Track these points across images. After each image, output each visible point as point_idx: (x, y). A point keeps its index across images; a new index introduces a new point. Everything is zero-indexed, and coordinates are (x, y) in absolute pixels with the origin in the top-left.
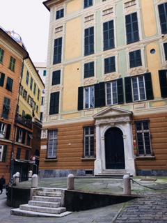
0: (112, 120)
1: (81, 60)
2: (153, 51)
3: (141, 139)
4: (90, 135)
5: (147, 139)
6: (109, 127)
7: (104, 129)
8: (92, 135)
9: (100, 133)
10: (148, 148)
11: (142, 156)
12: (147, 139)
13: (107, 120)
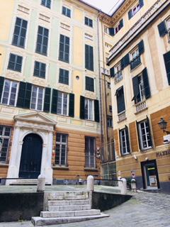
0: (36, 125)
1: (7, 47)
2: (77, 77)
4: (61, 143)
5: (63, 151)
6: (31, 132)
7: (26, 132)
8: (57, 143)
9: (18, 138)
10: (63, 159)
11: (57, 166)
12: (63, 151)
13: (31, 124)
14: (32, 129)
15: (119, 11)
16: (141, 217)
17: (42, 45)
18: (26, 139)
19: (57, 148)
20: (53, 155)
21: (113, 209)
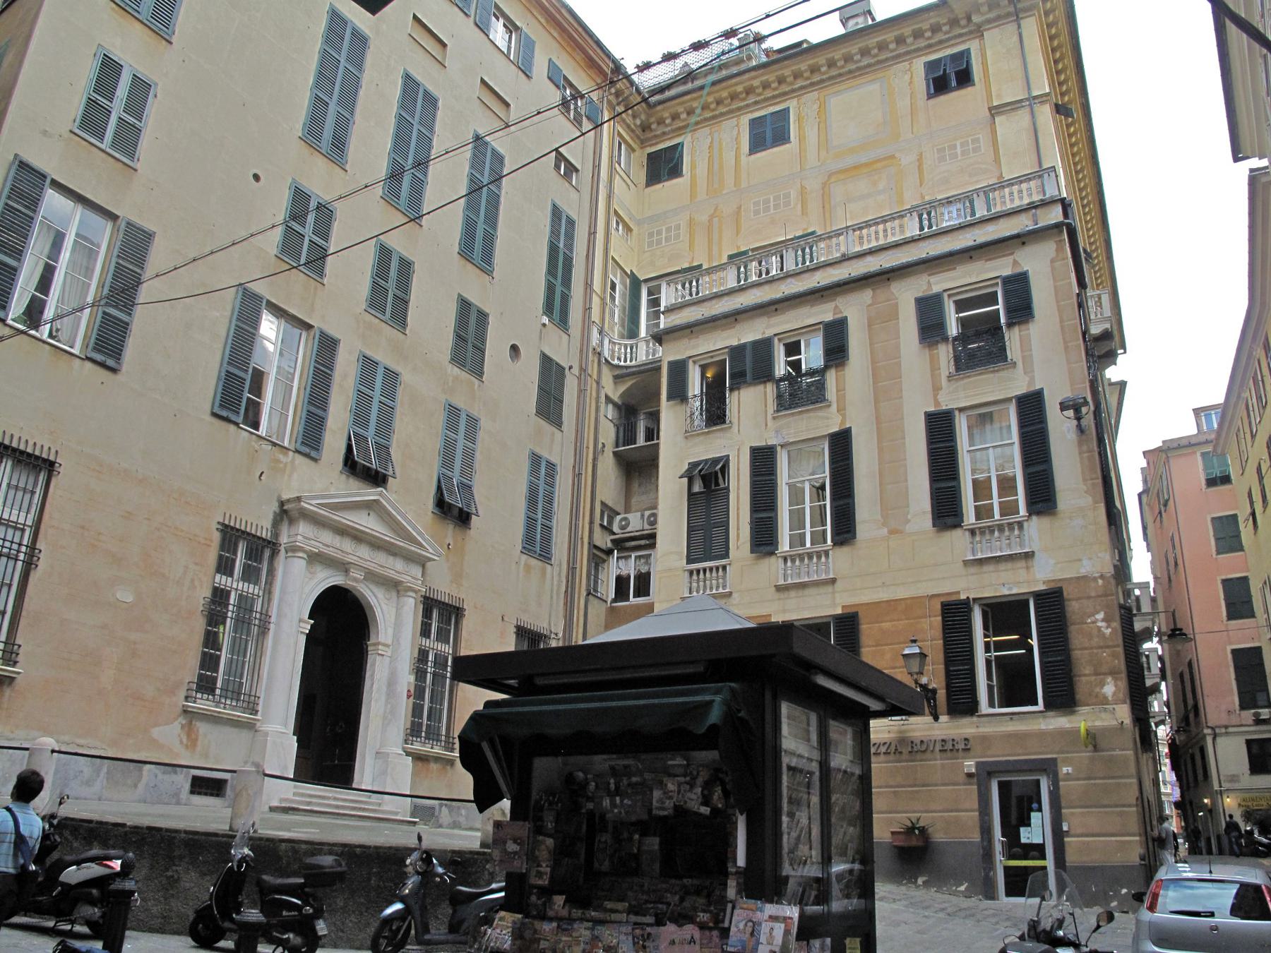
4: (235, 584)
7: (325, 579)
9: (294, 594)
11: (417, 747)
13: (347, 545)
14: (344, 567)
15: (1081, 135)
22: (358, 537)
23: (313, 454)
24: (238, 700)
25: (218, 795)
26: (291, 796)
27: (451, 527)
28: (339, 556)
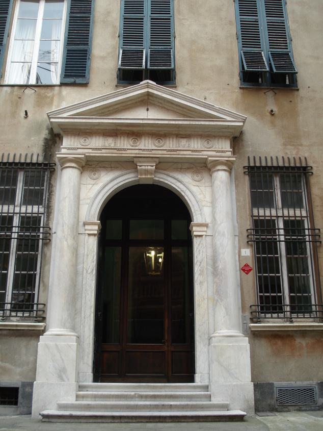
0: (147, 145)
3: (272, 246)
7: (104, 185)
8: (33, 209)
9: (77, 204)
14: (129, 164)
16: (65, 218)
17: (263, 20)
18: (116, 209)
19: (261, 235)
20: (245, 269)
21: (170, 189)
22: (135, 132)
23: (79, 80)
24: (11, 311)
25: (10, 403)
26: (71, 400)
27: (270, 94)
28: (115, 154)
